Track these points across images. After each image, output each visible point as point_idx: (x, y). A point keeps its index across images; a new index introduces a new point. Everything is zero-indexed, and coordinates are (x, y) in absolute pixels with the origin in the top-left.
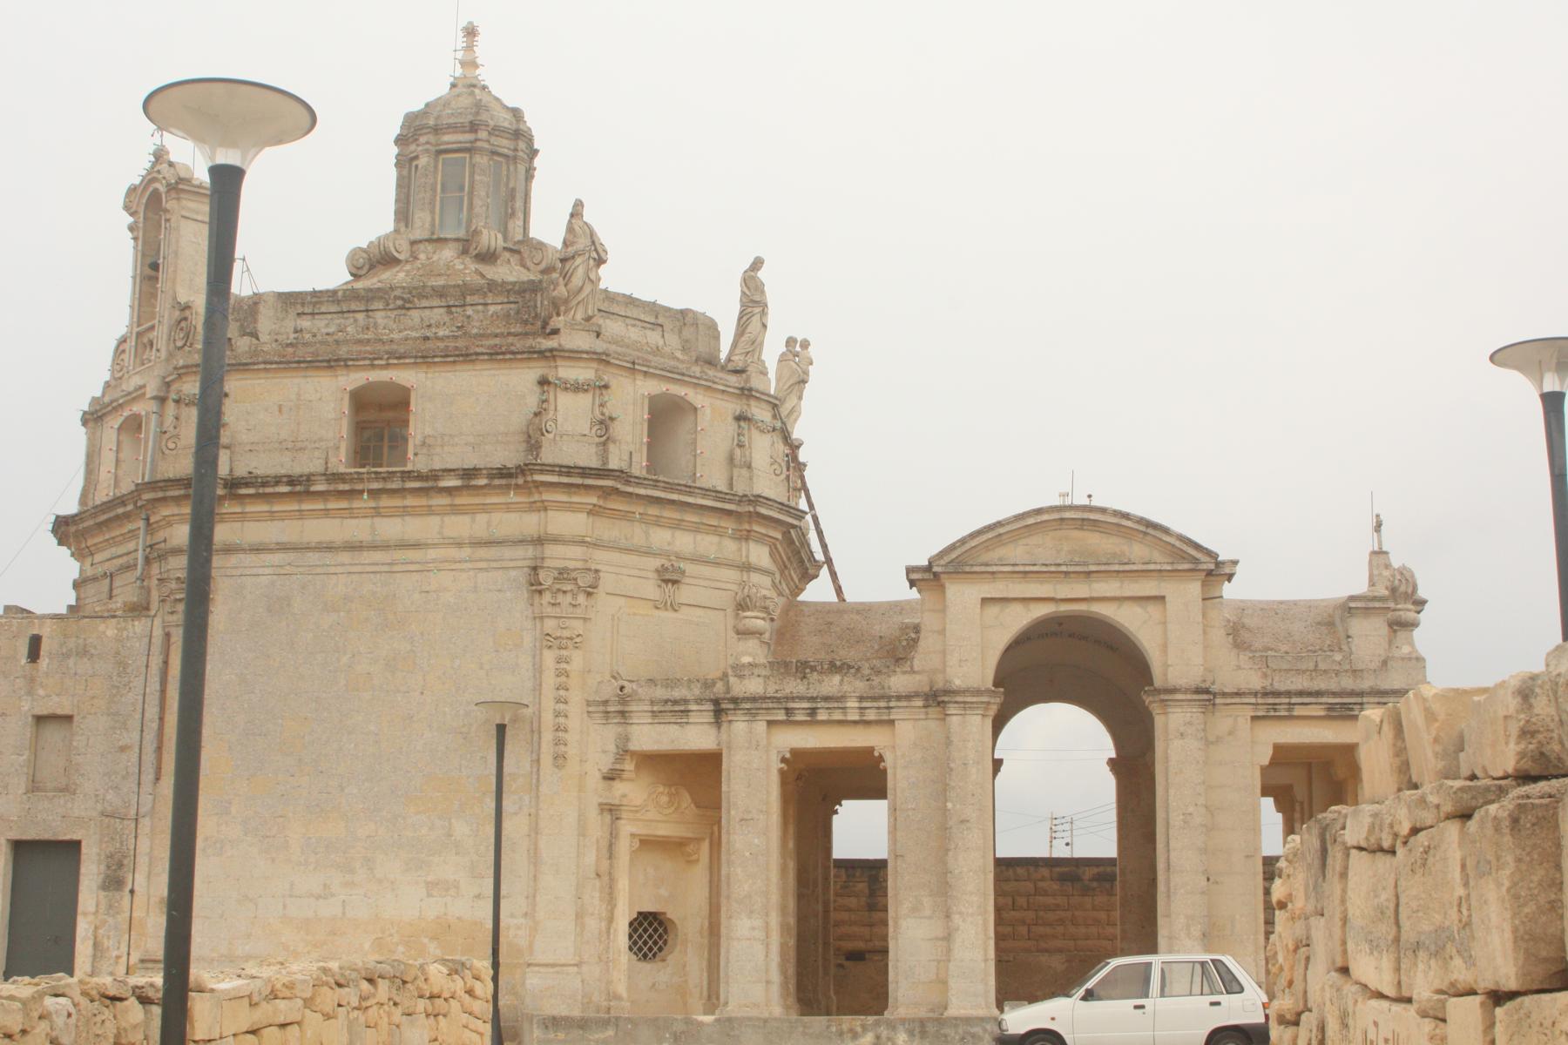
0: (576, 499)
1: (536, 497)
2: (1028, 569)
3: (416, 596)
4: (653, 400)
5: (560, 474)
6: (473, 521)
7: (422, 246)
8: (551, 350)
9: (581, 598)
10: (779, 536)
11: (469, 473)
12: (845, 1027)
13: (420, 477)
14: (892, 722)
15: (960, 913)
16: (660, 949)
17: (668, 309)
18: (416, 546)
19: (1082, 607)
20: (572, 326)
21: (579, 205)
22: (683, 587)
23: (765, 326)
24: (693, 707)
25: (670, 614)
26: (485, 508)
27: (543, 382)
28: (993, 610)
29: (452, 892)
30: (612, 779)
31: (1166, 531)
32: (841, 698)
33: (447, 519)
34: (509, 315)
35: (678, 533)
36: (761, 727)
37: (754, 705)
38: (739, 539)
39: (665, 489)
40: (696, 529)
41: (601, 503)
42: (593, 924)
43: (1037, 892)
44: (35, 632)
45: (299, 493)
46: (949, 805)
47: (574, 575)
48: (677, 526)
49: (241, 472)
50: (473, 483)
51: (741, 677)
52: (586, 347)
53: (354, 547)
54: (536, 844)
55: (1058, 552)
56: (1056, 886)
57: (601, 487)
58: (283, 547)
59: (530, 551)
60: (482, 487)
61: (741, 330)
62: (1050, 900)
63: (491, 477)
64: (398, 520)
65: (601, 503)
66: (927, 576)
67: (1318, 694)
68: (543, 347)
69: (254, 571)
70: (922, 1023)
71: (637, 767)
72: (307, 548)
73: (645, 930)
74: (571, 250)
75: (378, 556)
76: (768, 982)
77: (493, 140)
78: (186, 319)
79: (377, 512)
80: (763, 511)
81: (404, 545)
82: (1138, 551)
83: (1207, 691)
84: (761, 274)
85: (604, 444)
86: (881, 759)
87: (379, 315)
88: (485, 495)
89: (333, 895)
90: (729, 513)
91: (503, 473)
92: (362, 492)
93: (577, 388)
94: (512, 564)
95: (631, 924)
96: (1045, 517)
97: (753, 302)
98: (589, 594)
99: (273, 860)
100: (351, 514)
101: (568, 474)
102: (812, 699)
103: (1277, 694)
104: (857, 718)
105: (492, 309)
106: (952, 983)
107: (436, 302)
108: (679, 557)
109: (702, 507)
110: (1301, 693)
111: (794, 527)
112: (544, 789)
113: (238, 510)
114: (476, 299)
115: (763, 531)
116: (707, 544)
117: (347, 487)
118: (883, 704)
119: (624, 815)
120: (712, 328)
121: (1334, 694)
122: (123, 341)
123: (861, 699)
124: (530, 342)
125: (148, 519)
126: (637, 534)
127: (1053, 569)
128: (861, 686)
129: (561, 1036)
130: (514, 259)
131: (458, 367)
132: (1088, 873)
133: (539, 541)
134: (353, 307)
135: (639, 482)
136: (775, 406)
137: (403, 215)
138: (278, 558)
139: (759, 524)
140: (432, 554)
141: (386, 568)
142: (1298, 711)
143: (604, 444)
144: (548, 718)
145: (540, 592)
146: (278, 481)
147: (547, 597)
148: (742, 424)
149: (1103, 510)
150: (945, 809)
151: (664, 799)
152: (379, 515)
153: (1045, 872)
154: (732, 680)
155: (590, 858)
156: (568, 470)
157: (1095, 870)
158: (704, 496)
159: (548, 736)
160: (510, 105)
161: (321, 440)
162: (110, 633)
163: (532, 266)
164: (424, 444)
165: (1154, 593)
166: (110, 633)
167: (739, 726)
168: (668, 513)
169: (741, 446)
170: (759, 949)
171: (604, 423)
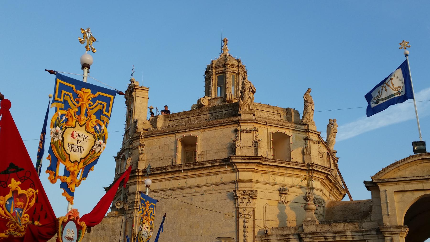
0: (248, 167)
2: (411, 179)
4: (274, 134)
6: (216, 177)
7: (211, 101)
8: (238, 120)
10: (323, 178)
11: (213, 161)
13: (199, 164)
18: (199, 186)
20: (246, 112)
24: (291, 237)
26: (220, 173)
32: (344, 232)
35: (286, 178)
39: (279, 163)
40: (292, 176)
45: (164, 173)
48: (286, 175)
51: (307, 225)
55: (423, 171)
59: (233, 186)
60: (218, 166)
63: (220, 162)
64: (194, 179)
66: (372, 185)
77: (231, 68)
79: (188, 177)
84: (310, 94)
87: (192, 118)
91: (224, 160)
92: (181, 170)
100: (179, 178)
101: (244, 159)
102: (334, 233)
105: (224, 112)
108: (286, 185)
111: (329, 175)
114: (219, 110)
117: (177, 169)
118: (360, 234)
123: (352, 232)
126: (271, 178)
127: (421, 178)
131: (211, 129)
133: (236, 182)
134: (184, 117)
135: (269, 160)
136: (319, 135)
140: (204, 189)
141: (190, 195)
146: (157, 169)
148: (307, 141)
154: (304, 226)
158: (293, 165)
168: (282, 171)
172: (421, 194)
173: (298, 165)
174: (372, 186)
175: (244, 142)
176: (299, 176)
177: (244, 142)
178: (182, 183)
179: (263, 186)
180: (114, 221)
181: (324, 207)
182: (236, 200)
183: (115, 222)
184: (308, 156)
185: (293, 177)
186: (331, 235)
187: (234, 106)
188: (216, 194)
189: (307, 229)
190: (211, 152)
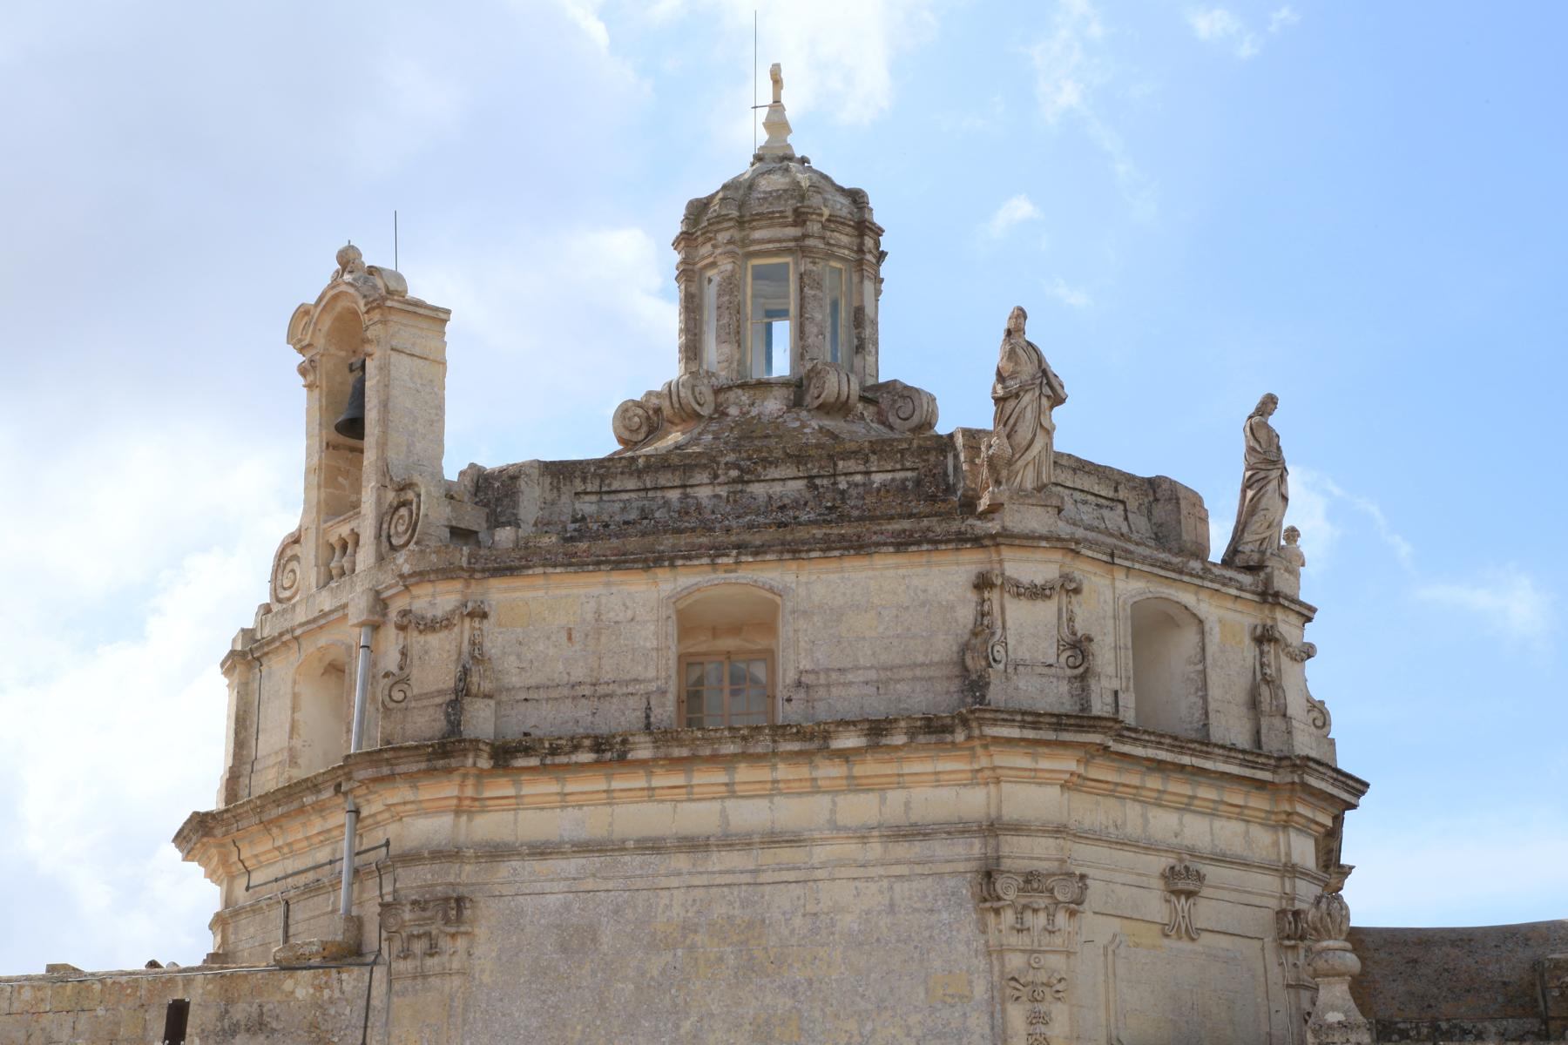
0: (1044, 764)
1: (984, 762)
3: (797, 921)
5: (1023, 725)
6: (883, 801)
7: (732, 395)
9: (1061, 918)
17: (1130, 478)
18: (794, 840)
21: (1020, 314)
22: (1202, 903)
23: (1285, 499)
25: (1185, 945)
26: (900, 782)
27: (983, 583)
33: (840, 799)
34: (905, 488)
35: (1188, 818)
38: (1274, 827)
44: (178, 996)
47: (1049, 882)
49: (513, 732)
50: (884, 741)
52: (1042, 530)
53: (694, 845)
57: (1083, 744)
58: (584, 848)
59: (977, 847)
65: (1081, 770)
68: (978, 532)
69: (538, 887)
72: (620, 847)
74: (1013, 384)
75: (734, 859)
78: (404, 504)
79: (731, 792)
80: (1314, 782)
81: (774, 839)
85: (1083, 678)
88: (901, 760)
90: (1261, 785)
93: (1037, 593)
94: (947, 868)
97: (1265, 464)
98: (1072, 914)
101: (1035, 726)
108: (1193, 853)
109: (1223, 775)
113: (511, 791)
114: (852, 465)
115: (1308, 813)
116: (1229, 834)
122: (295, 540)
124: (955, 526)
125: (357, 812)
126: (1132, 818)
130: (870, 412)
133: (993, 828)
137: (692, 350)
139: (1303, 801)
141: (747, 878)
145: (997, 911)
147: (1009, 917)
152: (733, 795)
156: (1032, 719)
160: (846, 186)
161: (636, 681)
162: (301, 993)
163: (897, 422)
164: (799, 684)
166: (301, 993)
168: (1179, 787)
169: (1267, 681)
175: (1020, 642)
176: (1240, 813)
177: (1020, 642)
178: (699, 816)
180: (319, 988)
182: (295, 847)
183: (326, 993)
184: (1278, 722)
185: (1213, 814)
187: (928, 451)
188: (885, 883)
190: (850, 677)
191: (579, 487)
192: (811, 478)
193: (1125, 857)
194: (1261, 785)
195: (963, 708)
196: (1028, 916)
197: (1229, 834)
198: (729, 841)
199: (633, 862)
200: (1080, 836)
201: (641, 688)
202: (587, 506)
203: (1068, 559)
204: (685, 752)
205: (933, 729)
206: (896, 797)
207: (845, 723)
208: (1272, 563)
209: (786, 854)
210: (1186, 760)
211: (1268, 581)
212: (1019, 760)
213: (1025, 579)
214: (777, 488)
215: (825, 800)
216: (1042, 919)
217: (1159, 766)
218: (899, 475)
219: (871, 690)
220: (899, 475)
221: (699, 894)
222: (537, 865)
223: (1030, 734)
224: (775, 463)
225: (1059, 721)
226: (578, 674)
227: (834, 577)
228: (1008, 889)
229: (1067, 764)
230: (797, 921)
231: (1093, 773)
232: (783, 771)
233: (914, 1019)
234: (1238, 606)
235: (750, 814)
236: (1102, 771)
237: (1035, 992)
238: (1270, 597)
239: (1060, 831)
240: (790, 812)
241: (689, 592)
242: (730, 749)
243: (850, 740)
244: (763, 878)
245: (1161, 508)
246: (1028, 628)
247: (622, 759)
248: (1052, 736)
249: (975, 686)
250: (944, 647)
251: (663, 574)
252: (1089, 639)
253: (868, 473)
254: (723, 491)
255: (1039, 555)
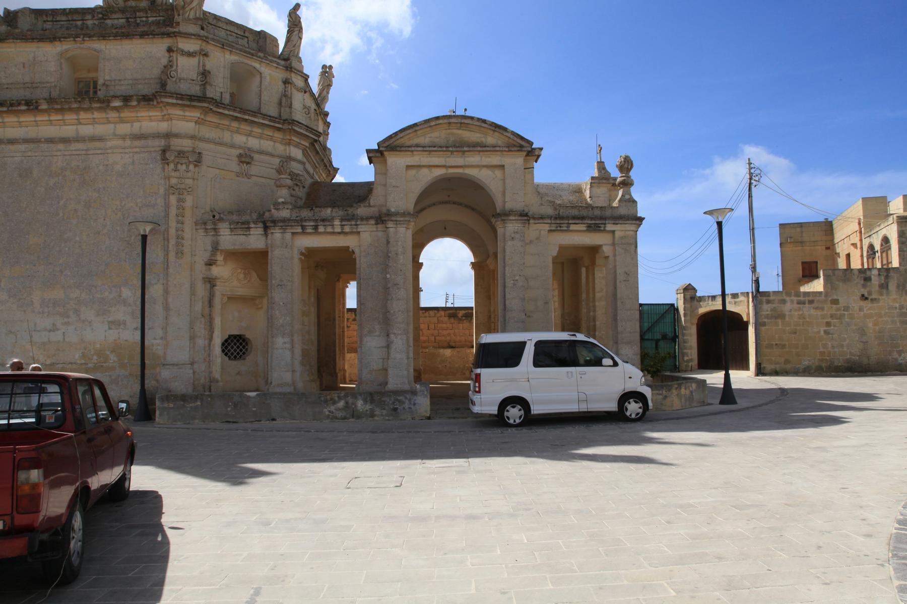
0: (187, 114)
1: (165, 112)
3: (101, 168)
6: (132, 126)
9: (191, 167)
10: (307, 145)
12: (328, 397)
14: (358, 233)
15: (395, 334)
16: (244, 353)
18: (100, 139)
19: (460, 171)
24: (252, 225)
25: (245, 180)
27: (170, 50)
28: (413, 172)
29: (122, 326)
30: (211, 265)
31: (505, 129)
33: (118, 126)
35: (250, 139)
36: (288, 236)
37: (285, 223)
38: (285, 144)
39: (240, 112)
41: (202, 117)
42: (201, 342)
43: (439, 322)
46: (388, 276)
53: (66, 141)
54: (166, 300)
56: (446, 319)
57: (202, 107)
58: (26, 141)
59: (163, 142)
61: (288, 40)
62: (444, 325)
65: (202, 117)
67: (583, 218)
69: (12, 154)
70: (371, 394)
71: (225, 259)
73: (235, 344)
75: (79, 146)
76: (293, 371)
80: (296, 129)
81: (93, 139)
82: (491, 139)
83: (526, 215)
85: (204, 85)
86: (353, 252)
89: (58, 330)
93: (190, 54)
95: (223, 344)
96: (441, 121)
97: (295, 25)
98: (196, 166)
99: (25, 311)
101: (182, 99)
102: (316, 221)
103: (562, 218)
104: (340, 230)
106: (390, 371)
107: (120, 16)
108: (249, 149)
110: (574, 218)
111: (316, 141)
112: (171, 270)
114: (142, 14)
116: (267, 145)
119: (218, 283)
120: (274, 40)
121: (592, 219)
123: (342, 220)
126: (227, 136)
128: (341, 213)
129: (171, 405)
132: (461, 313)
133: (168, 136)
138: (23, 147)
141: (84, 152)
142: (572, 227)
143: (204, 85)
144: (172, 231)
145: (168, 164)
147: (172, 166)
149: (472, 118)
150: (386, 278)
151: (242, 276)
152: (80, 124)
153: (442, 313)
155: (198, 307)
156: (181, 96)
157: (463, 312)
158: (263, 119)
159: (172, 242)
165: (499, 163)
167: (277, 234)
168: (245, 127)
169: (285, 96)
170: (288, 353)
171: (205, 74)
172: (442, 171)
173: (270, 121)
174: (375, 156)
176: (271, 138)
178: (68, 131)
179: (212, 146)
181: (304, 187)
184: (287, 109)
186: (312, 224)
189: (276, 214)
191: (45, 19)
192: (127, 18)
193: (223, 149)
194: (279, 129)
195: (158, 93)
196: (179, 166)
197: (267, 145)
198: (78, 139)
199: (44, 146)
200: (202, 139)
201: (48, 85)
202: (48, 25)
203: (204, 44)
204: (59, 107)
205: (147, 100)
206: (137, 125)
207: (115, 97)
208: (292, 58)
209: (98, 144)
210: (247, 117)
211: (291, 64)
212: (179, 112)
213: (186, 49)
214: (116, 22)
215: (112, 126)
216: (184, 167)
217: (236, 119)
218: (158, 18)
219: (129, 87)
220: (158, 18)
221: (68, 157)
222: (11, 147)
223: (180, 102)
224: (115, 13)
225: (192, 98)
226: (27, 79)
227: (119, 47)
228: (171, 156)
229: (196, 114)
230: (101, 168)
231: (208, 119)
232: (96, 115)
233: (139, 200)
234: (278, 70)
235: (86, 130)
236: (211, 118)
237: (179, 191)
238: (289, 68)
239: (193, 137)
240: (99, 129)
241: (67, 51)
242: (75, 106)
243: (117, 103)
244: (90, 152)
245: (262, 39)
246: (187, 67)
247: (37, 108)
248: (188, 103)
249: (163, 85)
250: (156, 72)
251: (57, 43)
252: (209, 72)
253: (147, 17)
254: (96, 22)
255: (192, 41)
